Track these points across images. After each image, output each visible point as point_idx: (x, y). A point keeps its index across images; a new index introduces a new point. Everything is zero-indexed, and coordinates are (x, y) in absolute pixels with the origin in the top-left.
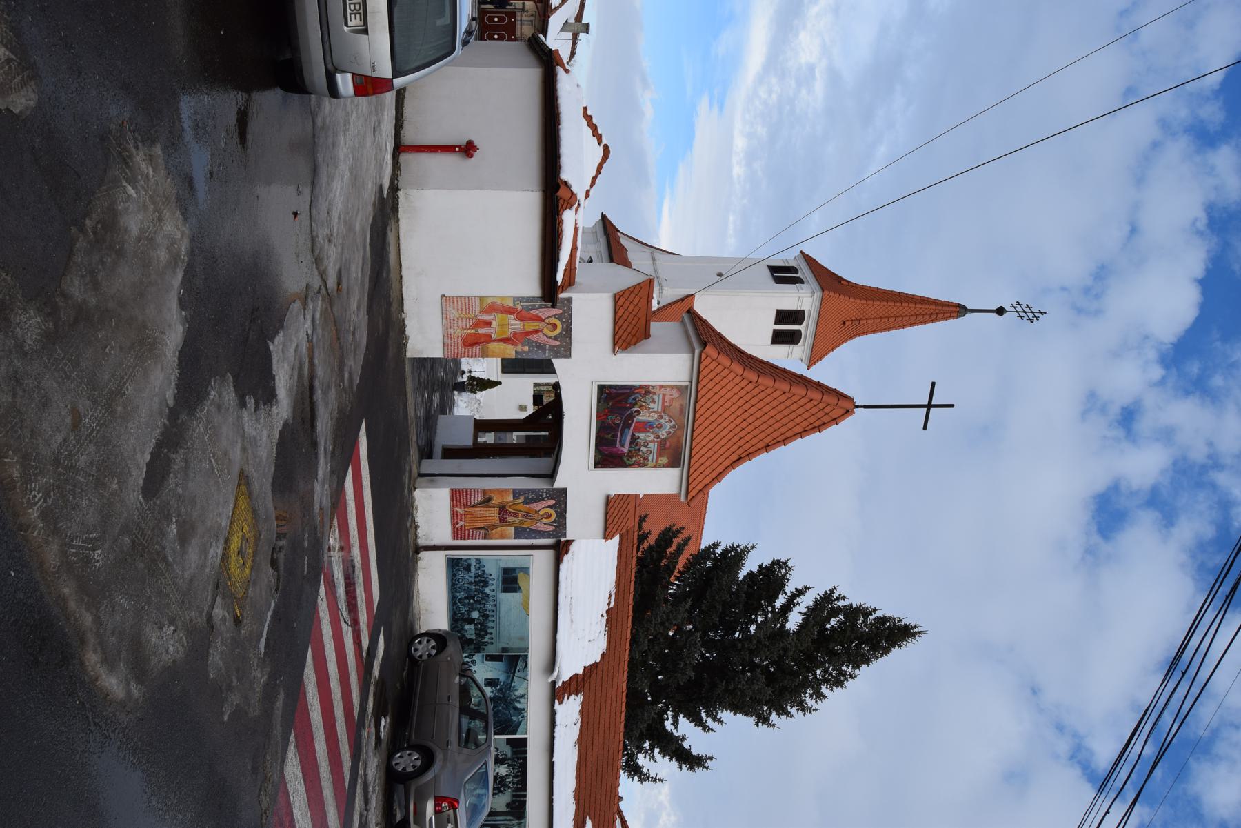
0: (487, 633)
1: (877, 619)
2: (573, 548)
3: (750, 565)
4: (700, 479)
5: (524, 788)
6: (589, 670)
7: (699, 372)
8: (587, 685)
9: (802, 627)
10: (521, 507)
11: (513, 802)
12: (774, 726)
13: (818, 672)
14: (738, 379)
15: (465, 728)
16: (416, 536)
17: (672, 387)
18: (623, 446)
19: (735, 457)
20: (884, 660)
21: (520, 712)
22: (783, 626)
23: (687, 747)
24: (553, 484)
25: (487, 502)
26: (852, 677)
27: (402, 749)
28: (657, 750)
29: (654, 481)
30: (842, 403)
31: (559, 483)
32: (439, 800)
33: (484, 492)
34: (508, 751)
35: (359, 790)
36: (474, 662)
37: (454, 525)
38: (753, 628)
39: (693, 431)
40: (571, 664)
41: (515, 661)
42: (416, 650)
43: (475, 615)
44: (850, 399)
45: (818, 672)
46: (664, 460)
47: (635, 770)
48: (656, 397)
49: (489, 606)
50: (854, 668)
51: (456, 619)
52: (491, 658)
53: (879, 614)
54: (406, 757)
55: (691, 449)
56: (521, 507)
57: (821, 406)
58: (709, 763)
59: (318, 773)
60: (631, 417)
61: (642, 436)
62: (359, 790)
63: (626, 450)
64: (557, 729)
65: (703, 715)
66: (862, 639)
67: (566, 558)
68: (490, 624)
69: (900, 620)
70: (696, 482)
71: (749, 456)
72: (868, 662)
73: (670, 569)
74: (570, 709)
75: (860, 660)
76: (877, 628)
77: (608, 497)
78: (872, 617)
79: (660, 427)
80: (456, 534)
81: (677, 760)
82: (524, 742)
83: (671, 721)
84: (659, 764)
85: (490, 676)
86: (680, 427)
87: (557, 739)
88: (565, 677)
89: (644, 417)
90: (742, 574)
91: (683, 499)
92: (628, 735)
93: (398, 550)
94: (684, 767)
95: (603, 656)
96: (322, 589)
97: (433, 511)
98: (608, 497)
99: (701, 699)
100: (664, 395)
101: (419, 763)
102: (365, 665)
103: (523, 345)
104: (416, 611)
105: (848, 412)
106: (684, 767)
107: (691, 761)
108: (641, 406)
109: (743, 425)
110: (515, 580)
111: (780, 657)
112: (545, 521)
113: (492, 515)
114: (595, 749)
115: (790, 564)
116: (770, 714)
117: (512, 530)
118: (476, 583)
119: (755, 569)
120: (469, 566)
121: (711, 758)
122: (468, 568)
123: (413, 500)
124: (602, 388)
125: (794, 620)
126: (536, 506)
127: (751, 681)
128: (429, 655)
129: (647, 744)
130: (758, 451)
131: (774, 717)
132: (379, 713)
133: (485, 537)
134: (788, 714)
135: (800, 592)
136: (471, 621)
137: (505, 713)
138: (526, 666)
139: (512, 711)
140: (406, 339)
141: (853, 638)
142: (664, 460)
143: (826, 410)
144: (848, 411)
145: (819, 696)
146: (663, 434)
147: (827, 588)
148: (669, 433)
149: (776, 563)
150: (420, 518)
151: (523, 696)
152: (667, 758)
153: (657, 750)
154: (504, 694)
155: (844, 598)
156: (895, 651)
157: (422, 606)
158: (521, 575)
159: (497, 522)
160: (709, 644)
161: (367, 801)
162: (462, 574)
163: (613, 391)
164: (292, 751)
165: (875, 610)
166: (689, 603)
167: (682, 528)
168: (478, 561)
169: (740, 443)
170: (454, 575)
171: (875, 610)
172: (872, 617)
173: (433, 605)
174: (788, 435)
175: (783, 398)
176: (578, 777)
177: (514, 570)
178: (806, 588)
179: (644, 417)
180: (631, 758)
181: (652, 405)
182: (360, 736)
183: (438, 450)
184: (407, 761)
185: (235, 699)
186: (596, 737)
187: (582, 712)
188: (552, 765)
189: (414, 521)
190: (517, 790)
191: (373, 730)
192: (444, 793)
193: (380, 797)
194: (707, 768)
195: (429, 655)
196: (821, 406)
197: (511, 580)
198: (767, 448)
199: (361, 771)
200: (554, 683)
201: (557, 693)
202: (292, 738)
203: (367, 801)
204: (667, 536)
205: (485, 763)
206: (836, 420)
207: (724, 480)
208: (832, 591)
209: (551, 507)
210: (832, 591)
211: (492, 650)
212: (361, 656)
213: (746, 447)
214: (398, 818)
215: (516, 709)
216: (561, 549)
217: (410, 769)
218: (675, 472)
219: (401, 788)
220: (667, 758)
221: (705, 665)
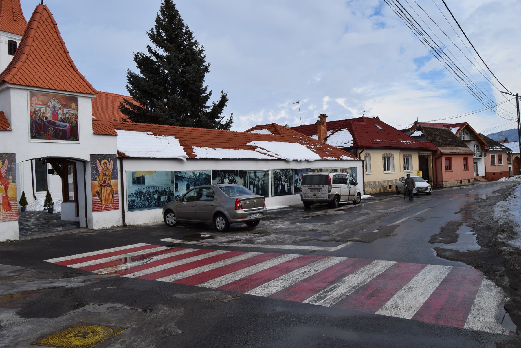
0: (165, 191)
1: (161, 14)
2: (122, 151)
3: (137, 72)
4: (83, 87)
5: (234, 171)
6: (182, 143)
7: (21, 85)
8: (189, 145)
9: (166, 49)
10: (101, 177)
11: (240, 176)
12: (209, 64)
13: (185, 43)
14: (25, 64)
15: (206, 198)
16: (118, 227)
17: (31, 100)
18: (66, 126)
19: (71, 69)
20: (180, 13)
21: (200, 174)
22: (165, 58)
23: (218, 103)
24: (88, 161)
25: (99, 194)
26: (188, 28)
27: (216, 227)
28: (219, 115)
29: (85, 111)
30: (40, 10)
31: (88, 159)
32: (237, 208)
33: (93, 195)
34: (218, 179)
35: (231, 245)
36: (179, 196)
37: (111, 209)
38: (166, 72)
39: (56, 90)
40: (179, 152)
41: (177, 177)
42: (172, 223)
43: (156, 196)
44: (38, 7)
45: (185, 43)
46: (73, 105)
47: (228, 125)
48: (37, 109)
49: (152, 190)
50: (184, 27)
51: (158, 205)
52: (176, 188)
53: (160, 13)
54: (219, 224)
55: (66, 91)
56: (101, 177)
57: (42, 22)
58: (225, 93)
59: (220, 268)
60: (49, 122)
61: (60, 116)
62: (231, 245)
63: (68, 125)
64: (208, 157)
65: (204, 95)
66: (171, 22)
67: (127, 154)
68: (160, 189)
69: (162, 4)
70: (85, 89)
71: (70, 62)
72: (181, 20)
73: (139, 109)
74: (200, 152)
75: (181, 24)
76: (166, 14)
77: (94, 134)
78: (161, 17)
79: (54, 107)
80: (116, 207)
81: (223, 107)
82: (214, 172)
83: (207, 110)
84: (225, 116)
85: (185, 188)
86: (54, 97)
87: (211, 157)
88: (185, 154)
89: (49, 115)
90: (142, 76)
91: (95, 97)
92: (213, 127)
93: (126, 234)
94: (226, 104)
95: (176, 138)
96: (128, 276)
97: (104, 220)
98: (94, 134)
99: (198, 97)
100: (36, 104)
101: (221, 218)
102: (173, 246)
103: (8, 179)
104: (155, 224)
105: (45, 8)
106: (226, 104)
107: (224, 101)
108: (43, 116)
109: (53, 64)
110: (138, 179)
111: (178, 59)
112: (108, 165)
113: (106, 191)
114: (217, 141)
115: (136, 53)
116: (204, 65)
117: (113, 181)
118: (141, 197)
119: (139, 70)
120: (132, 200)
121: (222, 92)
122: (133, 201)
123: (98, 230)
124: (33, 137)
125: (162, 52)
126: (100, 169)
127: (189, 73)
128: (174, 216)
129: (217, 120)
130: (68, 57)
131: (205, 64)
132: (198, 238)
133: (117, 194)
134: (204, 58)
135: (150, 50)
136: (159, 198)
137: (201, 181)
138: (180, 172)
139: (200, 178)
140: (8, 241)
141: (170, 28)
142: (73, 105)
143: (44, 19)
144: (45, 9)
145: (196, 43)
146: (58, 105)
147: (147, 36)
148: (58, 103)
149: (136, 60)
150: (108, 225)
151: (194, 173)
152: (222, 111)
153: (219, 115)
154: (193, 182)
155: (152, 29)
156: (176, 7)
157: (152, 221)
158: (136, 176)
159: (109, 188)
160: (174, 91)
161: (237, 241)
162: (136, 204)
163: (34, 131)
164: (206, 285)
165: (158, 15)
166: (154, 99)
167: (120, 103)
168: (129, 196)
169: (63, 66)
170: (137, 207)
171: (158, 15)
172: (161, 17)
173: (152, 216)
174: (58, 41)
175: (37, 42)
176: (229, 148)
177: (133, 179)
178: (148, 46)
179: (49, 115)
180: (222, 127)
181: (42, 111)
182: (207, 247)
183: (77, 219)
184: (220, 223)
185: (172, 326)
186: (212, 141)
187: (201, 147)
188: (224, 160)
189: (110, 229)
190: (235, 174)
191: (205, 240)
192: (233, 206)
193: (235, 234)
194: (227, 94)
195: (174, 216)
196: (42, 22)
197: (139, 180)
198: (66, 52)
199: (223, 245)
200: (187, 159)
201: (192, 158)
202: (200, 285)
203: (237, 241)
204: (124, 110)
205: (221, 188)
206: (50, 15)
207: (84, 75)
208: (149, 34)
209: (100, 162)
210: (149, 34)
211: (173, 188)
212: (168, 250)
213: (65, 63)
214: (245, 225)
215: (199, 176)
216: (122, 157)
217: (224, 222)
218: (80, 100)
219: (231, 225)
220: (222, 111)
221: (183, 95)
